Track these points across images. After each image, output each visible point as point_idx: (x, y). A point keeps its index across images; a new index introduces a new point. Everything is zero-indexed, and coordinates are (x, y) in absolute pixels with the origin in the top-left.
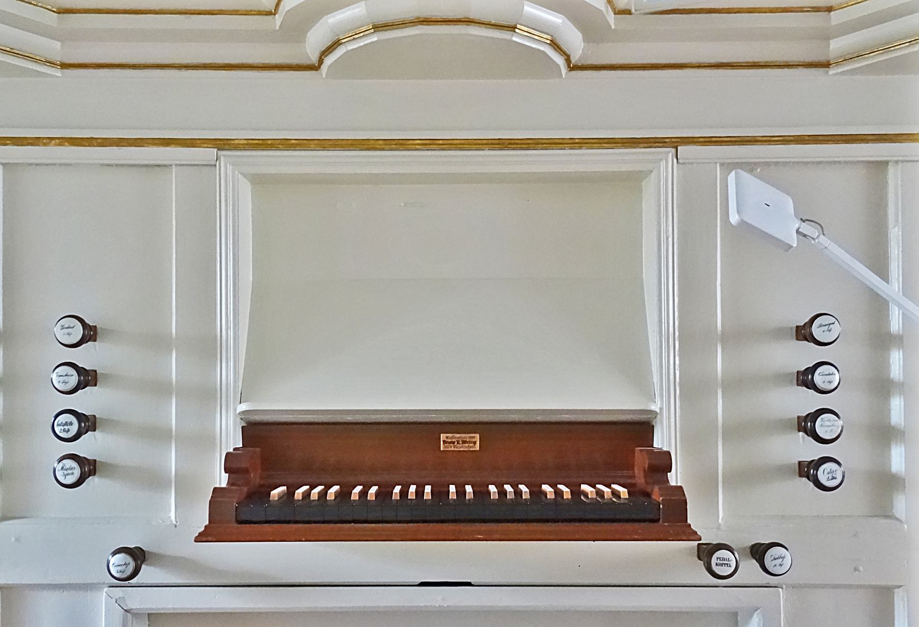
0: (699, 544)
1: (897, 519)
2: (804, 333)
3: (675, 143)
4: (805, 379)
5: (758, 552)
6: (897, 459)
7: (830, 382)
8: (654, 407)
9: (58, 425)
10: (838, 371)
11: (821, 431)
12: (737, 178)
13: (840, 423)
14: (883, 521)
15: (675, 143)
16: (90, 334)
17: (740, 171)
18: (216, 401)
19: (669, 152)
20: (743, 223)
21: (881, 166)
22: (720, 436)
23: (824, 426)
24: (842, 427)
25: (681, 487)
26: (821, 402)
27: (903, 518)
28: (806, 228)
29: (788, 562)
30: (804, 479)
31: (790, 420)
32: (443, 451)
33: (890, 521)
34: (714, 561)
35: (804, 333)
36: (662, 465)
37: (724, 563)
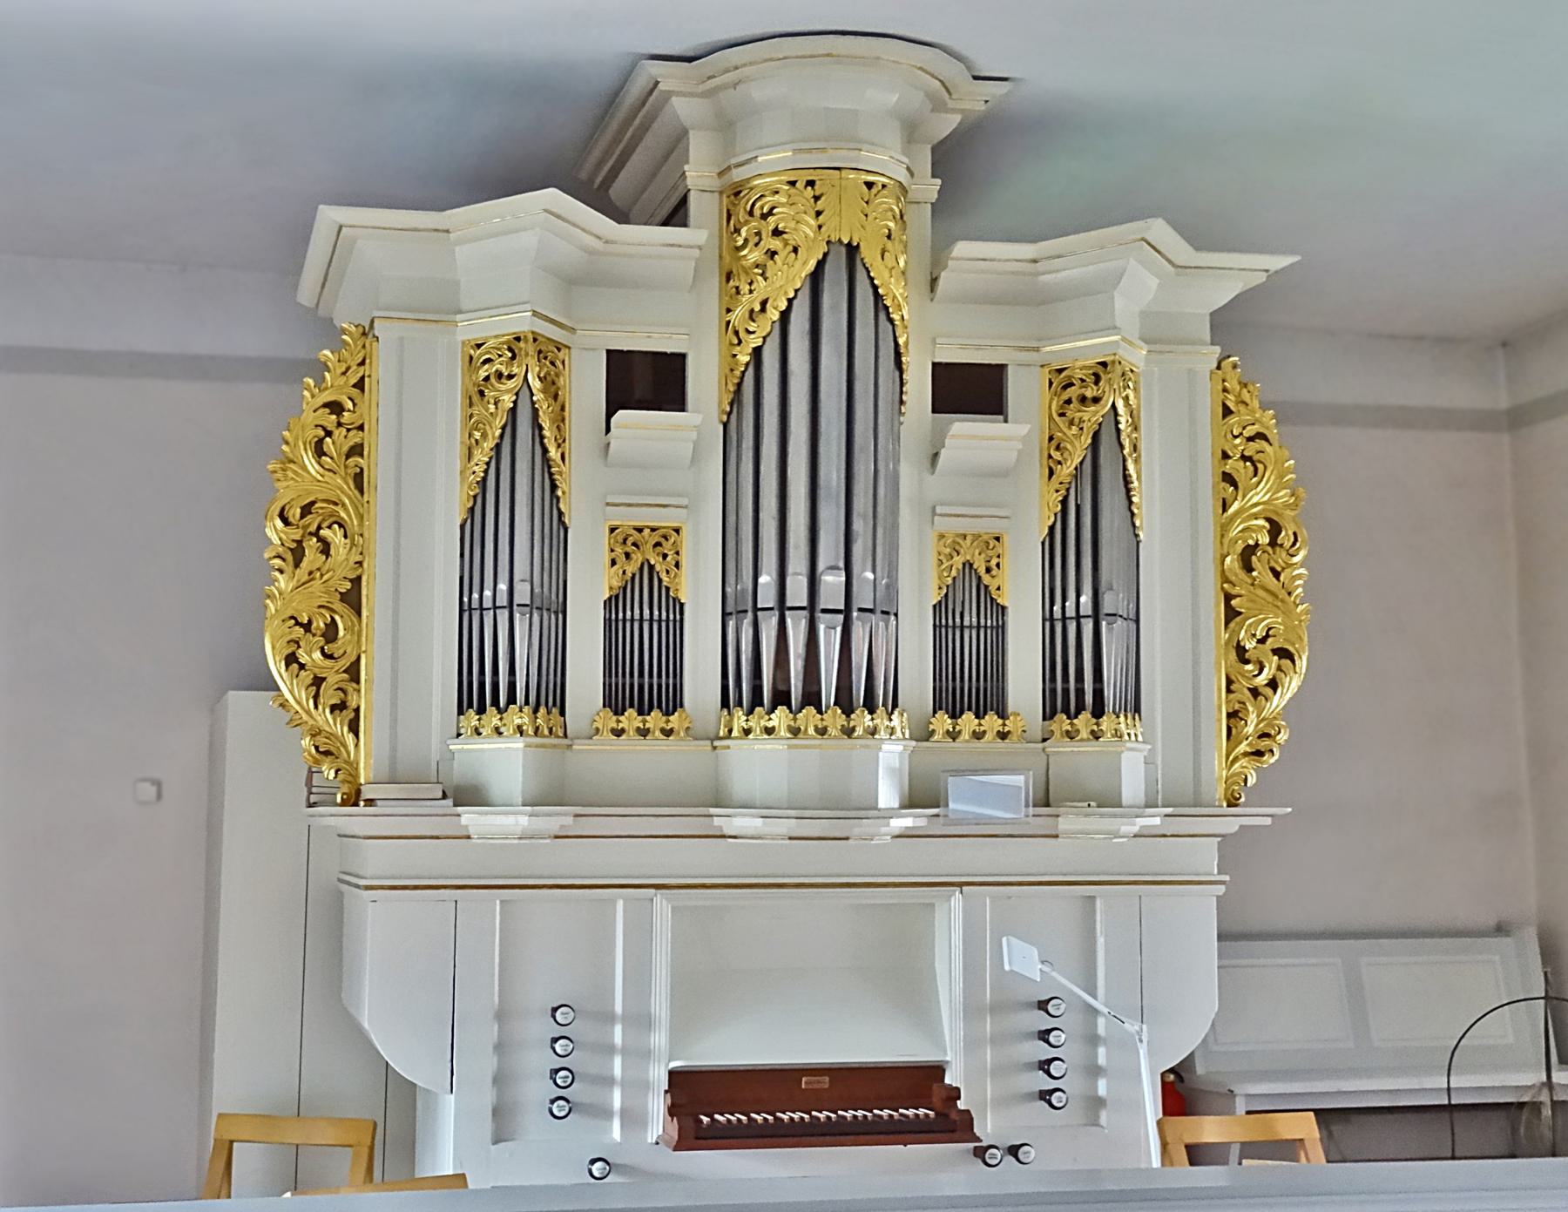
0: (976, 1147)
1: (1102, 1127)
2: (1043, 1005)
3: (961, 885)
4: (1044, 1035)
5: (1014, 1151)
6: (1102, 1088)
7: (1028, 1157)
8: (948, 1059)
9: (560, 1078)
10: (1062, 1031)
11: (1053, 1072)
12: (1008, 939)
13: (1065, 1066)
14: (1094, 1128)
15: (961, 885)
16: (1045, 1096)
17: (1010, 937)
18: (650, 1059)
19: (955, 891)
20: (1012, 971)
21: (1092, 899)
22: (989, 1075)
23: (1055, 1069)
24: (1066, 1069)
25: (968, 1111)
26: (1053, 1053)
27: (1105, 1126)
28: (1046, 969)
29: (1033, 1155)
30: (1043, 1102)
31: (1034, 1063)
32: (806, 1089)
33: (1098, 1128)
34: (987, 1156)
35: (1043, 1005)
36: (955, 1094)
37: (993, 1156)
